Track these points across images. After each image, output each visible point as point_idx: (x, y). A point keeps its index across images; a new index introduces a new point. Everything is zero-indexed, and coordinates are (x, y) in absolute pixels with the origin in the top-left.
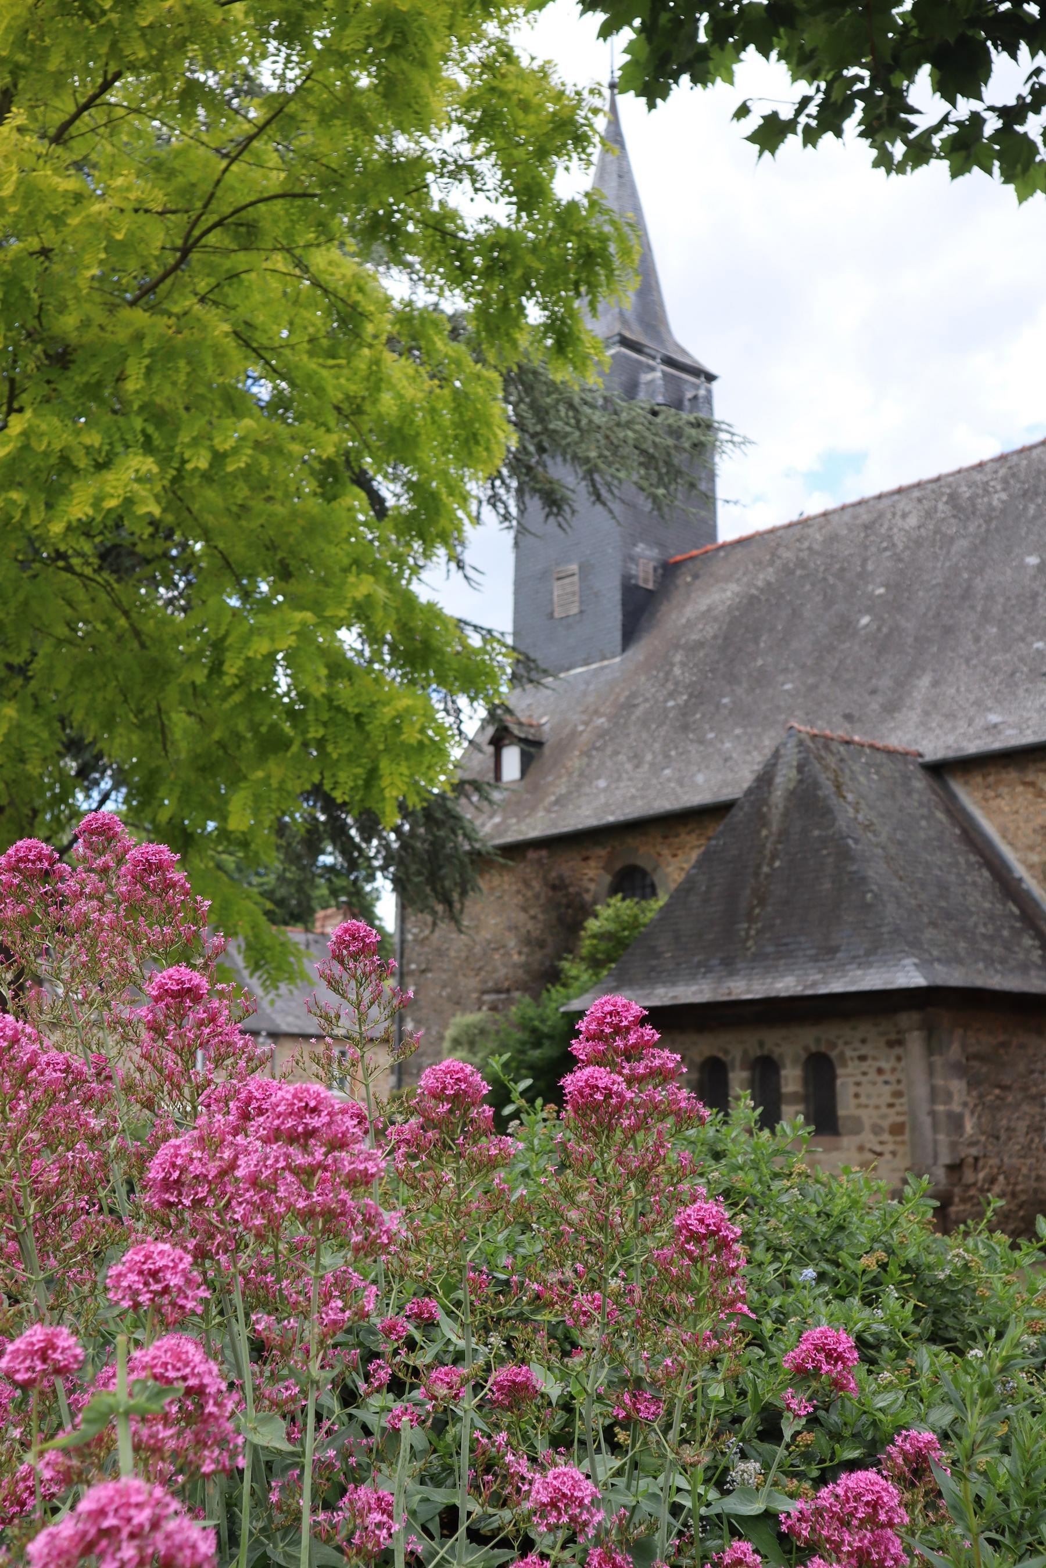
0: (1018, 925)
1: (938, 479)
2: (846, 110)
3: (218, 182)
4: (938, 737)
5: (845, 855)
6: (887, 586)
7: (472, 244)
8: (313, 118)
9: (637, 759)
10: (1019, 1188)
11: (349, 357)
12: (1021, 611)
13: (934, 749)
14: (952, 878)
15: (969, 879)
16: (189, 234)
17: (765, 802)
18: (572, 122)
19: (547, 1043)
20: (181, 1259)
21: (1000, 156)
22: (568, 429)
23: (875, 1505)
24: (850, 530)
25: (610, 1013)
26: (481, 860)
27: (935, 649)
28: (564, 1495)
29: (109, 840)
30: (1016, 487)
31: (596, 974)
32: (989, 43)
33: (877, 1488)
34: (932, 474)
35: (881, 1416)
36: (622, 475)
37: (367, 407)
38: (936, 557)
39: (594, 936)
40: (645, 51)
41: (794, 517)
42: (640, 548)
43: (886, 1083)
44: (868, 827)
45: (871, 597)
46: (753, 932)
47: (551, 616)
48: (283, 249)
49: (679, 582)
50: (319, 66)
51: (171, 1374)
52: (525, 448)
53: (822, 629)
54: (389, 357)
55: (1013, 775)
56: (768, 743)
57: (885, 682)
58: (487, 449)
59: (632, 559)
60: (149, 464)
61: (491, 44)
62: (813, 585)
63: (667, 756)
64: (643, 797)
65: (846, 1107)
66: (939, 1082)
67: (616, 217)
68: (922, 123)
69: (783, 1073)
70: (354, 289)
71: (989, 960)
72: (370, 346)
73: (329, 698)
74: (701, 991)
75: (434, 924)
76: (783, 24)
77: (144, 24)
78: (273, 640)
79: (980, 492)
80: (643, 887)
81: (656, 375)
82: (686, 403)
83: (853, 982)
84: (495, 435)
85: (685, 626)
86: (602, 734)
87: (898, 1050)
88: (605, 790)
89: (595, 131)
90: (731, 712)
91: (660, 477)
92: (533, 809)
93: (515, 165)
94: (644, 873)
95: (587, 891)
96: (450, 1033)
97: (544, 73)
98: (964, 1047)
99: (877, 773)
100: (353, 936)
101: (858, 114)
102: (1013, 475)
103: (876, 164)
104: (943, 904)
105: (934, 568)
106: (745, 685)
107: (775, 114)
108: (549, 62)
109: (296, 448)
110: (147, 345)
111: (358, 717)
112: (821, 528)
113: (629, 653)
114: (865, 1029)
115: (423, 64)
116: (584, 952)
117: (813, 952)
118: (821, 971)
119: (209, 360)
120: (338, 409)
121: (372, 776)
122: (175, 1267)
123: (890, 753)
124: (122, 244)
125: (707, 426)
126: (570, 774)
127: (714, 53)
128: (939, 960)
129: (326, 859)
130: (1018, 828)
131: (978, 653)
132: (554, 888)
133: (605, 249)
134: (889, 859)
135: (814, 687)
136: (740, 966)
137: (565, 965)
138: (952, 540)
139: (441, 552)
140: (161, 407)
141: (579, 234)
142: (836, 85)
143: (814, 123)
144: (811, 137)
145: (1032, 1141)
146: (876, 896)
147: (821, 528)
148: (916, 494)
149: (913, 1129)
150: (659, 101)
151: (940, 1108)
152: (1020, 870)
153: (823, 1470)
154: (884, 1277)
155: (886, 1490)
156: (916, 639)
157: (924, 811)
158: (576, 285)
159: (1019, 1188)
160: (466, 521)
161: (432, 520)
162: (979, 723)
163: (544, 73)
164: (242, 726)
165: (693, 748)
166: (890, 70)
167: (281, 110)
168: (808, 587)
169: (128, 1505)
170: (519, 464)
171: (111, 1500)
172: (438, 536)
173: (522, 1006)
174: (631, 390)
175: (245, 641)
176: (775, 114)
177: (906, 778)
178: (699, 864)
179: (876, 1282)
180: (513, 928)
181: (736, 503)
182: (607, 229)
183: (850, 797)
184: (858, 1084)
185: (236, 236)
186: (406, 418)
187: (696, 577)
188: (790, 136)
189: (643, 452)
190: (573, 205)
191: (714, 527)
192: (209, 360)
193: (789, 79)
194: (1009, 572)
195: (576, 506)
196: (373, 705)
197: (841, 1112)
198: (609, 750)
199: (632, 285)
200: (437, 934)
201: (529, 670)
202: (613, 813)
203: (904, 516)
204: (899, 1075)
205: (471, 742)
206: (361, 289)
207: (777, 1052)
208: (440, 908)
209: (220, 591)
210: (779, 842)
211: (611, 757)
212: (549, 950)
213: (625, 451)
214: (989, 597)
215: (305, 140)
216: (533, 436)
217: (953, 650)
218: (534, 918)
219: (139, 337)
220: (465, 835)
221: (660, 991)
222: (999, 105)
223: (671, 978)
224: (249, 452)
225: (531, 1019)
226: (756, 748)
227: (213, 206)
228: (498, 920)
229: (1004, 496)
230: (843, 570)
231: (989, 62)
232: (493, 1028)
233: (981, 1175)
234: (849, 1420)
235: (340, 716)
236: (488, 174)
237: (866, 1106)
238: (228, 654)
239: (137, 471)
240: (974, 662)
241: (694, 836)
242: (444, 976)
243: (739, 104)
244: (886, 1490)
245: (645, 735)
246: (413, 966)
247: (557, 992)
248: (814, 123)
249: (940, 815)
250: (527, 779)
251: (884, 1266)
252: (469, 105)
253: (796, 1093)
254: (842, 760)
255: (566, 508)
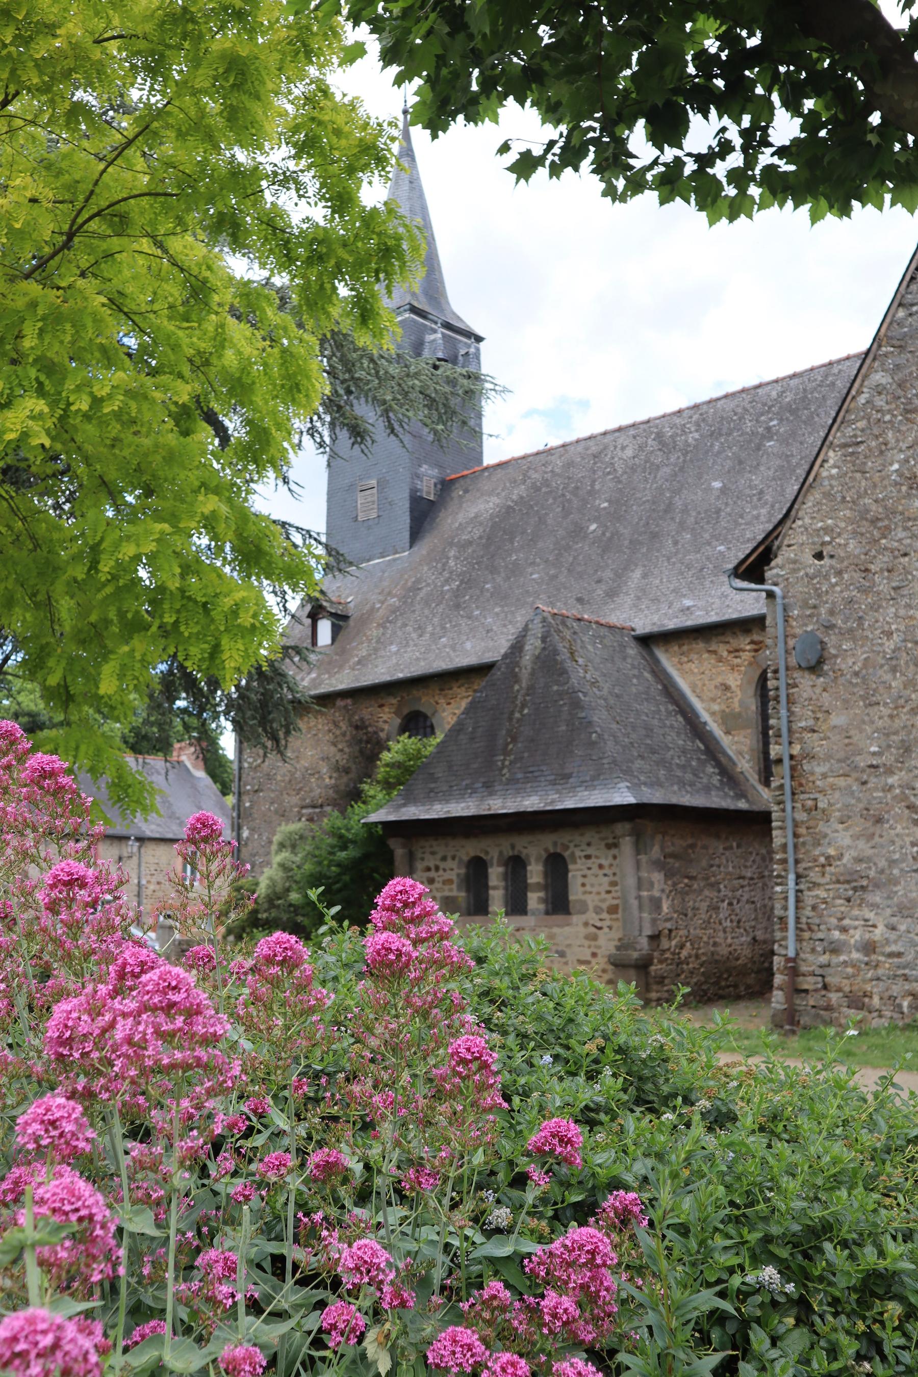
0: (703, 757)
1: (648, 422)
2: (581, 153)
3: (96, 183)
4: (646, 616)
5: (576, 705)
6: (609, 501)
7: (297, 237)
8: (172, 134)
9: (421, 630)
10: (701, 951)
11: (200, 322)
12: (708, 523)
13: (644, 624)
14: (656, 722)
15: (668, 723)
16: (74, 221)
17: (517, 664)
18: (374, 147)
19: (351, 846)
20: (74, 1109)
21: (696, 191)
22: (369, 378)
23: (593, 1253)
24: (583, 458)
25: (401, 892)
26: (300, 707)
27: (644, 550)
28: (366, 1262)
29: (12, 743)
30: (705, 428)
31: (389, 794)
32: (688, 107)
33: (595, 1240)
34: (644, 417)
35: (598, 1170)
36: (410, 414)
37: (214, 360)
38: (646, 480)
39: (387, 765)
40: (430, 96)
41: (541, 448)
42: (424, 468)
43: (605, 875)
44: (594, 684)
45: (598, 509)
46: (507, 763)
47: (356, 519)
48: (148, 235)
49: (454, 495)
50: (178, 95)
51: (67, 1208)
52: (336, 391)
53: (561, 533)
54: (231, 321)
55: (701, 645)
56: (520, 618)
57: (608, 574)
58: (307, 396)
59: (418, 476)
60: (41, 406)
61: (312, 82)
62: (555, 499)
63: (443, 628)
64: (425, 659)
65: (575, 894)
66: (645, 875)
67: (408, 222)
68: (637, 164)
69: (529, 868)
70: (204, 267)
71: (682, 783)
72: (217, 313)
73: (182, 591)
74: (468, 807)
75: (265, 756)
76: (535, 82)
77: (38, 56)
78: (138, 545)
79: (679, 432)
80: (425, 728)
81: (437, 336)
82: (460, 358)
83: (582, 801)
84: (313, 386)
85: (457, 529)
86: (394, 610)
87: (614, 851)
88: (396, 653)
89: (392, 154)
90: (492, 595)
91: (440, 417)
92: (341, 667)
93: (329, 177)
94: (425, 717)
95: (382, 730)
96: (277, 838)
97: (353, 106)
98: (662, 848)
99: (601, 643)
100: (203, 824)
101: (591, 156)
102: (704, 420)
103: (605, 194)
104: (649, 742)
105: (645, 488)
106: (503, 575)
107: (529, 152)
108: (357, 98)
109: (158, 395)
110: (40, 312)
111: (205, 605)
112: (561, 456)
113: (415, 549)
114: (590, 835)
115: (258, 98)
116: (380, 777)
117: (553, 777)
118: (558, 792)
119: (90, 324)
120: (190, 361)
121: (216, 650)
122: (70, 1115)
123: (611, 627)
124: (21, 231)
125: (475, 377)
126: (370, 641)
127: (483, 100)
128: (645, 784)
129: (181, 704)
130: (704, 685)
131: (676, 553)
132: (357, 727)
133: (399, 246)
134: (609, 708)
135: (555, 577)
136: (497, 788)
137: (365, 787)
138: (658, 468)
139: (271, 474)
140: (51, 360)
141: (379, 234)
142: (575, 133)
143: (556, 158)
144: (555, 171)
145: (711, 917)
146: (599, 736)
147: (561, 456)
148: (632, 432)
149: (624, 910)
150: (440, 133)
151: (645, 894)
152: (705, 716)
153: (556, 1210)
154: (602, 1058)
155: (601, 1241)
156: (631, 542)
157: (636, 672)
158: (377, 272)
159: (701, 951)
160: (290, 451)
161: (263, 450)
162: (677, 606)
163: (353, 106)
164: (112, 615)
165: (462, 622)
166: (616, 123)
167: (147, 127)
168: (551, 501)
169: (35, 1332)
170: (331, 404)
171: (22, 1329)
172: (268, 462)
173: (332, 819)
174: (418, 348)
175: (117, 546)
176: (529, 152)
177: (623, 647)
178: (467, 712)
179: (596, 1061)
180: (326, 759)
181: (497, 437)
182: (401, 230)
183: (581, 661)
184: (584, 876)
185: (111, 225)
186: (245, 369)
187: (466, 491)
188: (540, 168)
189: (427, 396)
190: (375, 210)
191: (481, 454)
192: (90, 324)
193: (540, 122)
194: (700, 493)
195: (375, 437)
196: (216, 595)
197: (572, 897)
198: (399, 623)
199: (420, 273)
200: (267, 763)
201: (339, 562)
202: (402, 671)
203: (623, 448)
204: (614, 869)
205: (293, 616)
206: (209, 268)
207: (525, 852)
208: (269, 744)
209: (97, 505)
210: (528, 695)
211: (400, 628)
212: (352, 775)
213: (412, 396)
214: (685, 511)
215: (168, 149)
216: (343, 382)
217: (658, 551)
218: (341, 750)
219: (33, 305)
220: (289, 688)
221: (437, 807)
222: (695, 152)
223: (447, 797)
224: (121, 398)
225: (339, 828)
226: (510, 622)
227: (93, 200)
228: (314, 752)
229: (696, 435)
230: (577, 488)
231: (688, 121)
232: (308, 834)
233: (674, 943)
234: (576, 1173)
235: (191, 604)
236: (310, 184)
237: (590, 893)
238: (103, 556)
239: (32, 411)
240: (674, 560)
241: (463, 689)
242: (272, 795)
243: (502, 142)
244: (601, 1241)
245: (426, 612)
246: (248, 787)
247: (359, 808)
248: (556, 158)
249: (647, 675)
250: (336, 643)
251: (602, 1050)
252: (296, 129)
253: (538, 883)
254: (575, 633)
255: (368, 438)
